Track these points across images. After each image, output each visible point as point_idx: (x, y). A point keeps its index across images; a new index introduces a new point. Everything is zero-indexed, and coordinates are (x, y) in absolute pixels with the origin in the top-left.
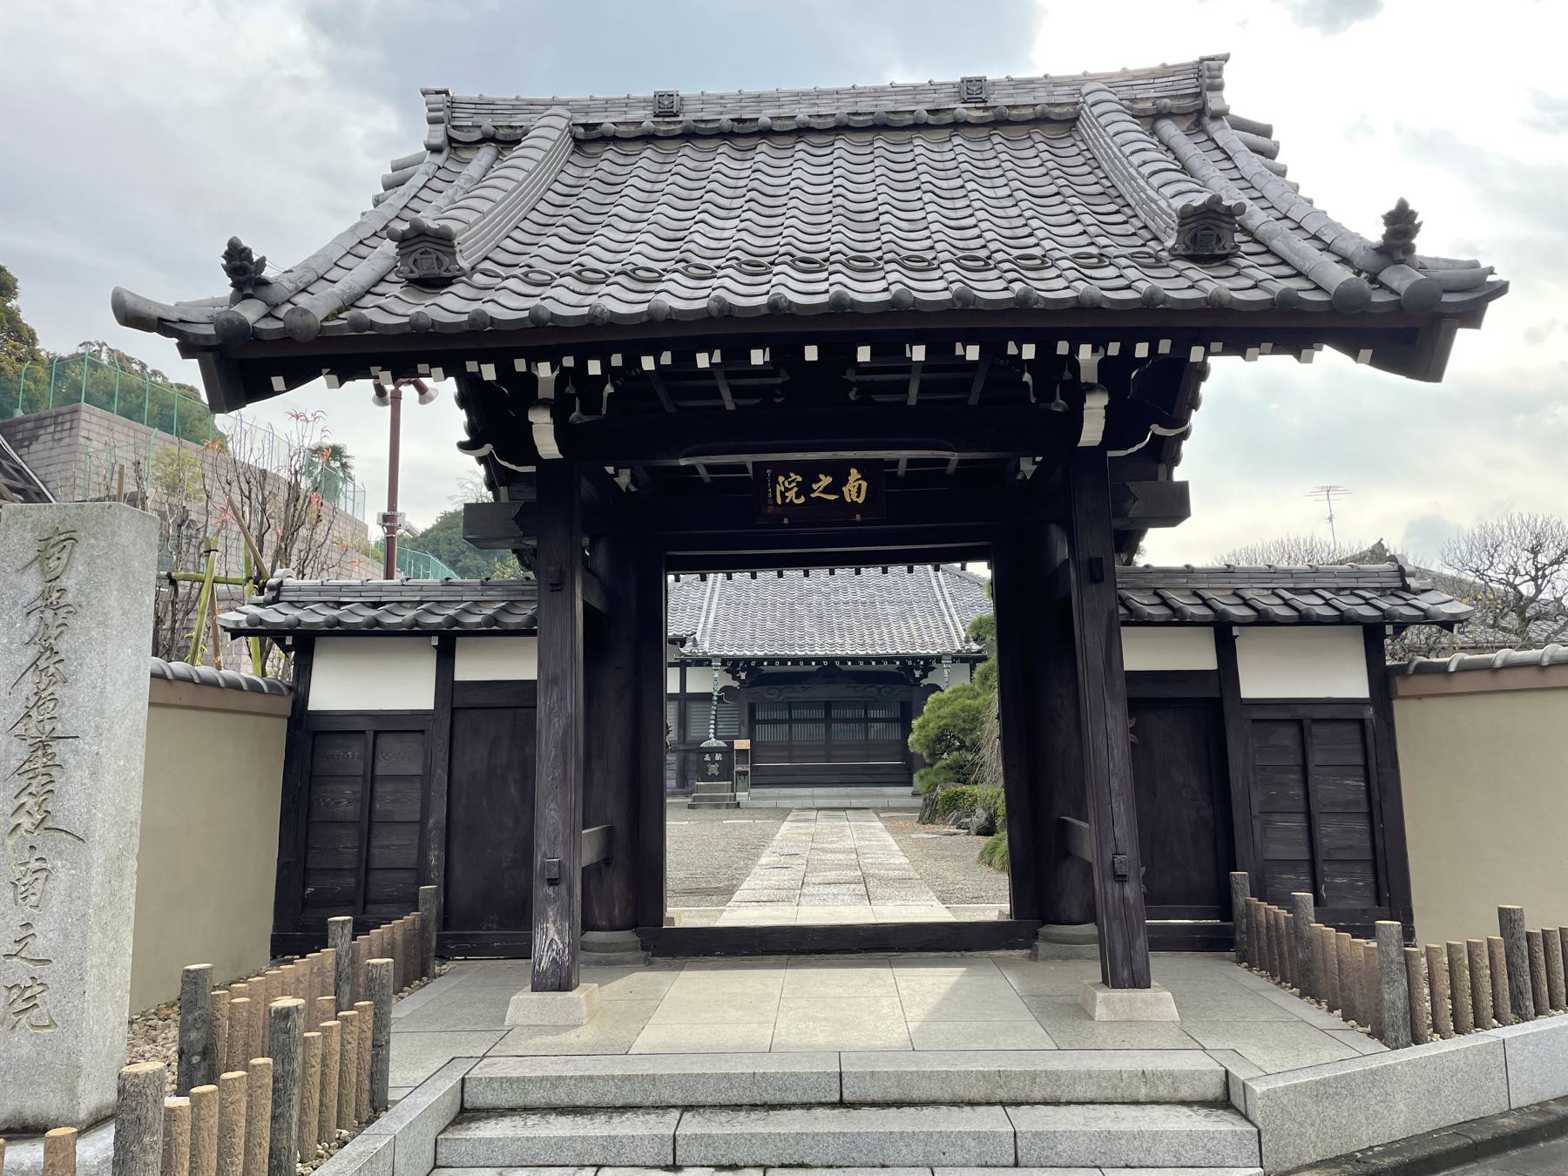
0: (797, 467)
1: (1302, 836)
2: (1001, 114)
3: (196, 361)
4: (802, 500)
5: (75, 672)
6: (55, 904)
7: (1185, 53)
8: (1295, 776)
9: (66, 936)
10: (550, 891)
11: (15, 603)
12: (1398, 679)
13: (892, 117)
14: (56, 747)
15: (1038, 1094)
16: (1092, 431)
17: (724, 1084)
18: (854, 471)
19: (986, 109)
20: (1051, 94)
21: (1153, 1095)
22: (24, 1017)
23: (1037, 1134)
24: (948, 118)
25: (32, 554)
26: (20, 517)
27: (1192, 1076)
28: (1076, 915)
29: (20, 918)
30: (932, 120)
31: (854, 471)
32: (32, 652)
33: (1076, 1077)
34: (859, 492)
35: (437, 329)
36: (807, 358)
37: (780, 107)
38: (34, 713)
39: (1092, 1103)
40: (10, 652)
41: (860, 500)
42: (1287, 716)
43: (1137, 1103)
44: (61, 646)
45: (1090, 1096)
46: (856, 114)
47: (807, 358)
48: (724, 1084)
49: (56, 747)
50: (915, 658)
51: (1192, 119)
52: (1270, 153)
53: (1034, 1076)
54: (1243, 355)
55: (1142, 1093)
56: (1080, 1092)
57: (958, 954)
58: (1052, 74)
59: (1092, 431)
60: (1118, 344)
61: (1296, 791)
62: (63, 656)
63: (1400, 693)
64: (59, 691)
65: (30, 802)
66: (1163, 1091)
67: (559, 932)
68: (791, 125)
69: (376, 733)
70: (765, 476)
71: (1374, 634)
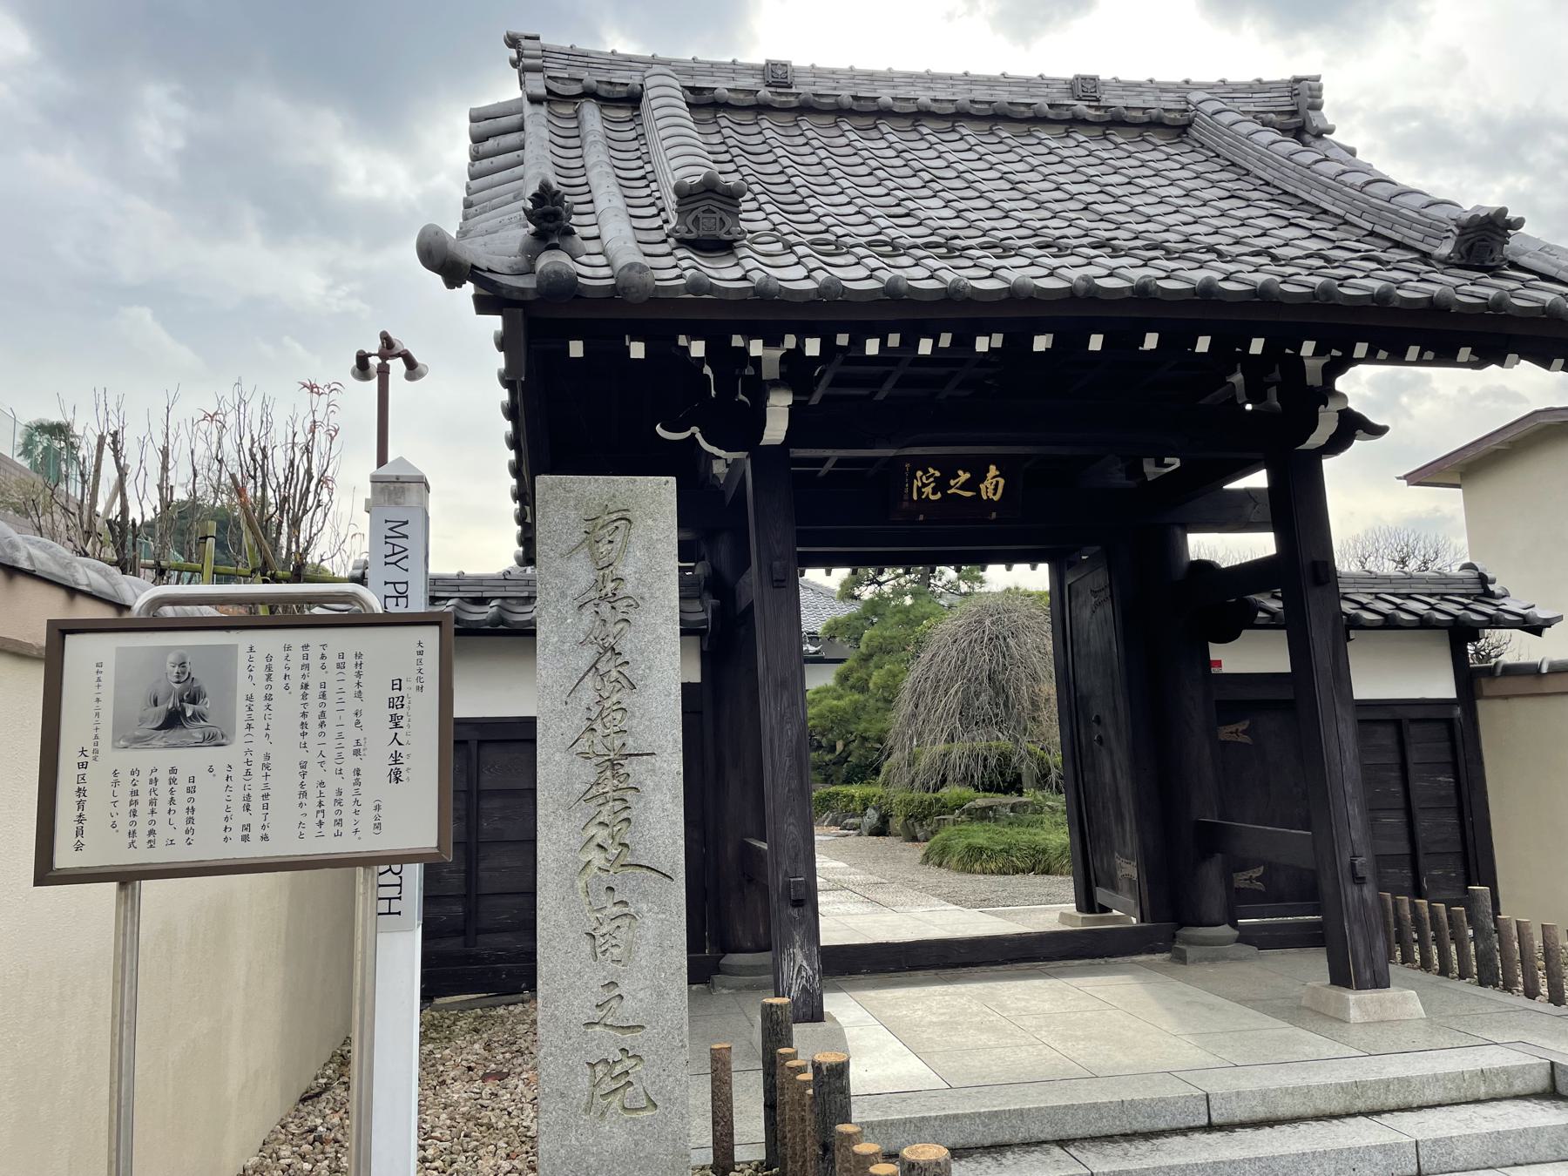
0: (935, 461)
1: (1402, 832)
2: (1120, 114)
3: (499, 318)
4: (939, 495)
5: (643, 677)
6: (643, 956)
8: (1395, 774)
9: (660, 995)
10: (795, 912)
11: (563, 595)
12: (1484, 681)
13: (1014, 108)
14: (630, 766)
15: (1392, 1102)
17: (1093, 1115)
18: (993, 468)
19: (1098, 108)
20: (1158, 99)
21: (1492, 1093)
22: (615, 1101)
23: (1436, 1141)
24: (1067, 115)
25: (578, 536)
26: (560, 491)
27: (1523, 1070)
28: (1216, 917)
29: (602, 976)
30: (1051, 114)
31: (993, 468)
32: (589, 654)
33: (1426, 1081)
34: (996, 490)
35: (782, 297)
36: (572, 355)
37: (894, 87)
38: (598, 726)
39: (1440, 1105)
40: (562, 653)
41: (996, 498)
42: (1388, 717)
43: (1477, 1101)
44: (625, 646)
45: (1437, 1099)
47: (572, 355)
48: (1093, 1115)
53: (1387, 1084)
54: (1501, 363)
55: (1482, 1092)
56: (1431, 1095)
57: (1102, 961)
58: (1158, 79)
60: (1252, 352)
61: (1397, 788)
62: (627, 658)
63: (1486, 692)
64: (627, 699)
65: (602, 835)
66: (1500, 1088)
67: (807, 957)
68: (911, 108)
69: (481, 743)
70: (896, 474)
71: (1461, 634)
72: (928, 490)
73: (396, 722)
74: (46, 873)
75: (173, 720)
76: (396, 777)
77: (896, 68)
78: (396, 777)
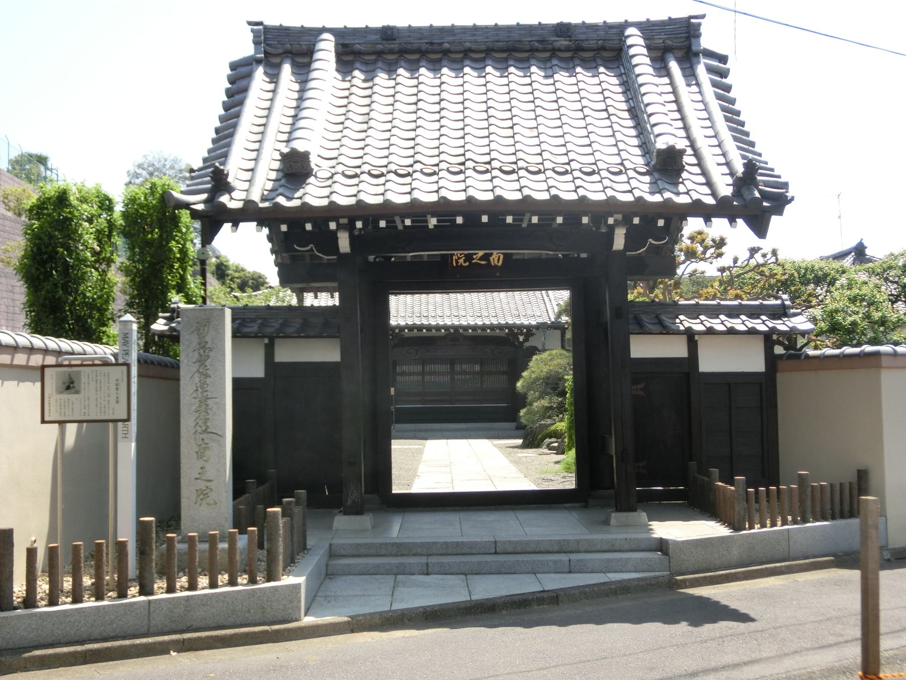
4: (467, 264)
7: (680, 12)
16: (619, 243)
34: (499, 260)
46: (498, 41)
49: (210, 402)
50: (520, 327)
51: (684, 51)
52: (724, 74)
59: (619, 243)
72: (461, 261)
73: (117, 389)
74: (43, 421)
75: (68, 388)
76: (117, 402)
77: (456, 24)
78: (117, 402)
